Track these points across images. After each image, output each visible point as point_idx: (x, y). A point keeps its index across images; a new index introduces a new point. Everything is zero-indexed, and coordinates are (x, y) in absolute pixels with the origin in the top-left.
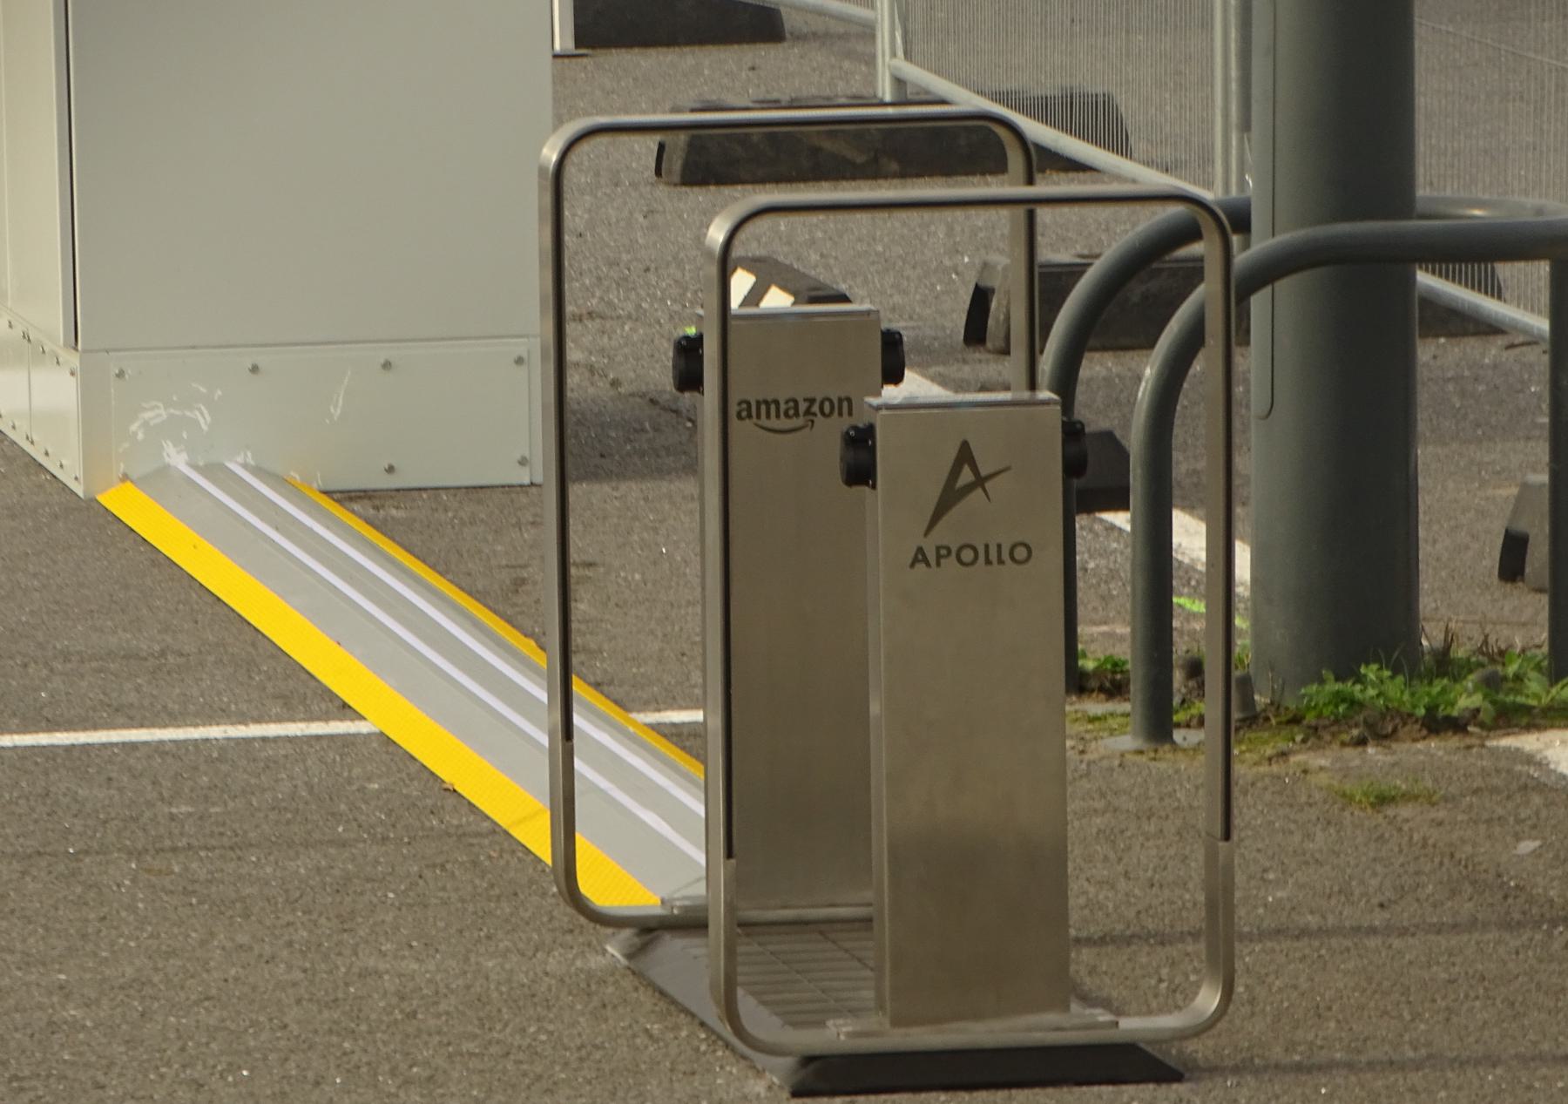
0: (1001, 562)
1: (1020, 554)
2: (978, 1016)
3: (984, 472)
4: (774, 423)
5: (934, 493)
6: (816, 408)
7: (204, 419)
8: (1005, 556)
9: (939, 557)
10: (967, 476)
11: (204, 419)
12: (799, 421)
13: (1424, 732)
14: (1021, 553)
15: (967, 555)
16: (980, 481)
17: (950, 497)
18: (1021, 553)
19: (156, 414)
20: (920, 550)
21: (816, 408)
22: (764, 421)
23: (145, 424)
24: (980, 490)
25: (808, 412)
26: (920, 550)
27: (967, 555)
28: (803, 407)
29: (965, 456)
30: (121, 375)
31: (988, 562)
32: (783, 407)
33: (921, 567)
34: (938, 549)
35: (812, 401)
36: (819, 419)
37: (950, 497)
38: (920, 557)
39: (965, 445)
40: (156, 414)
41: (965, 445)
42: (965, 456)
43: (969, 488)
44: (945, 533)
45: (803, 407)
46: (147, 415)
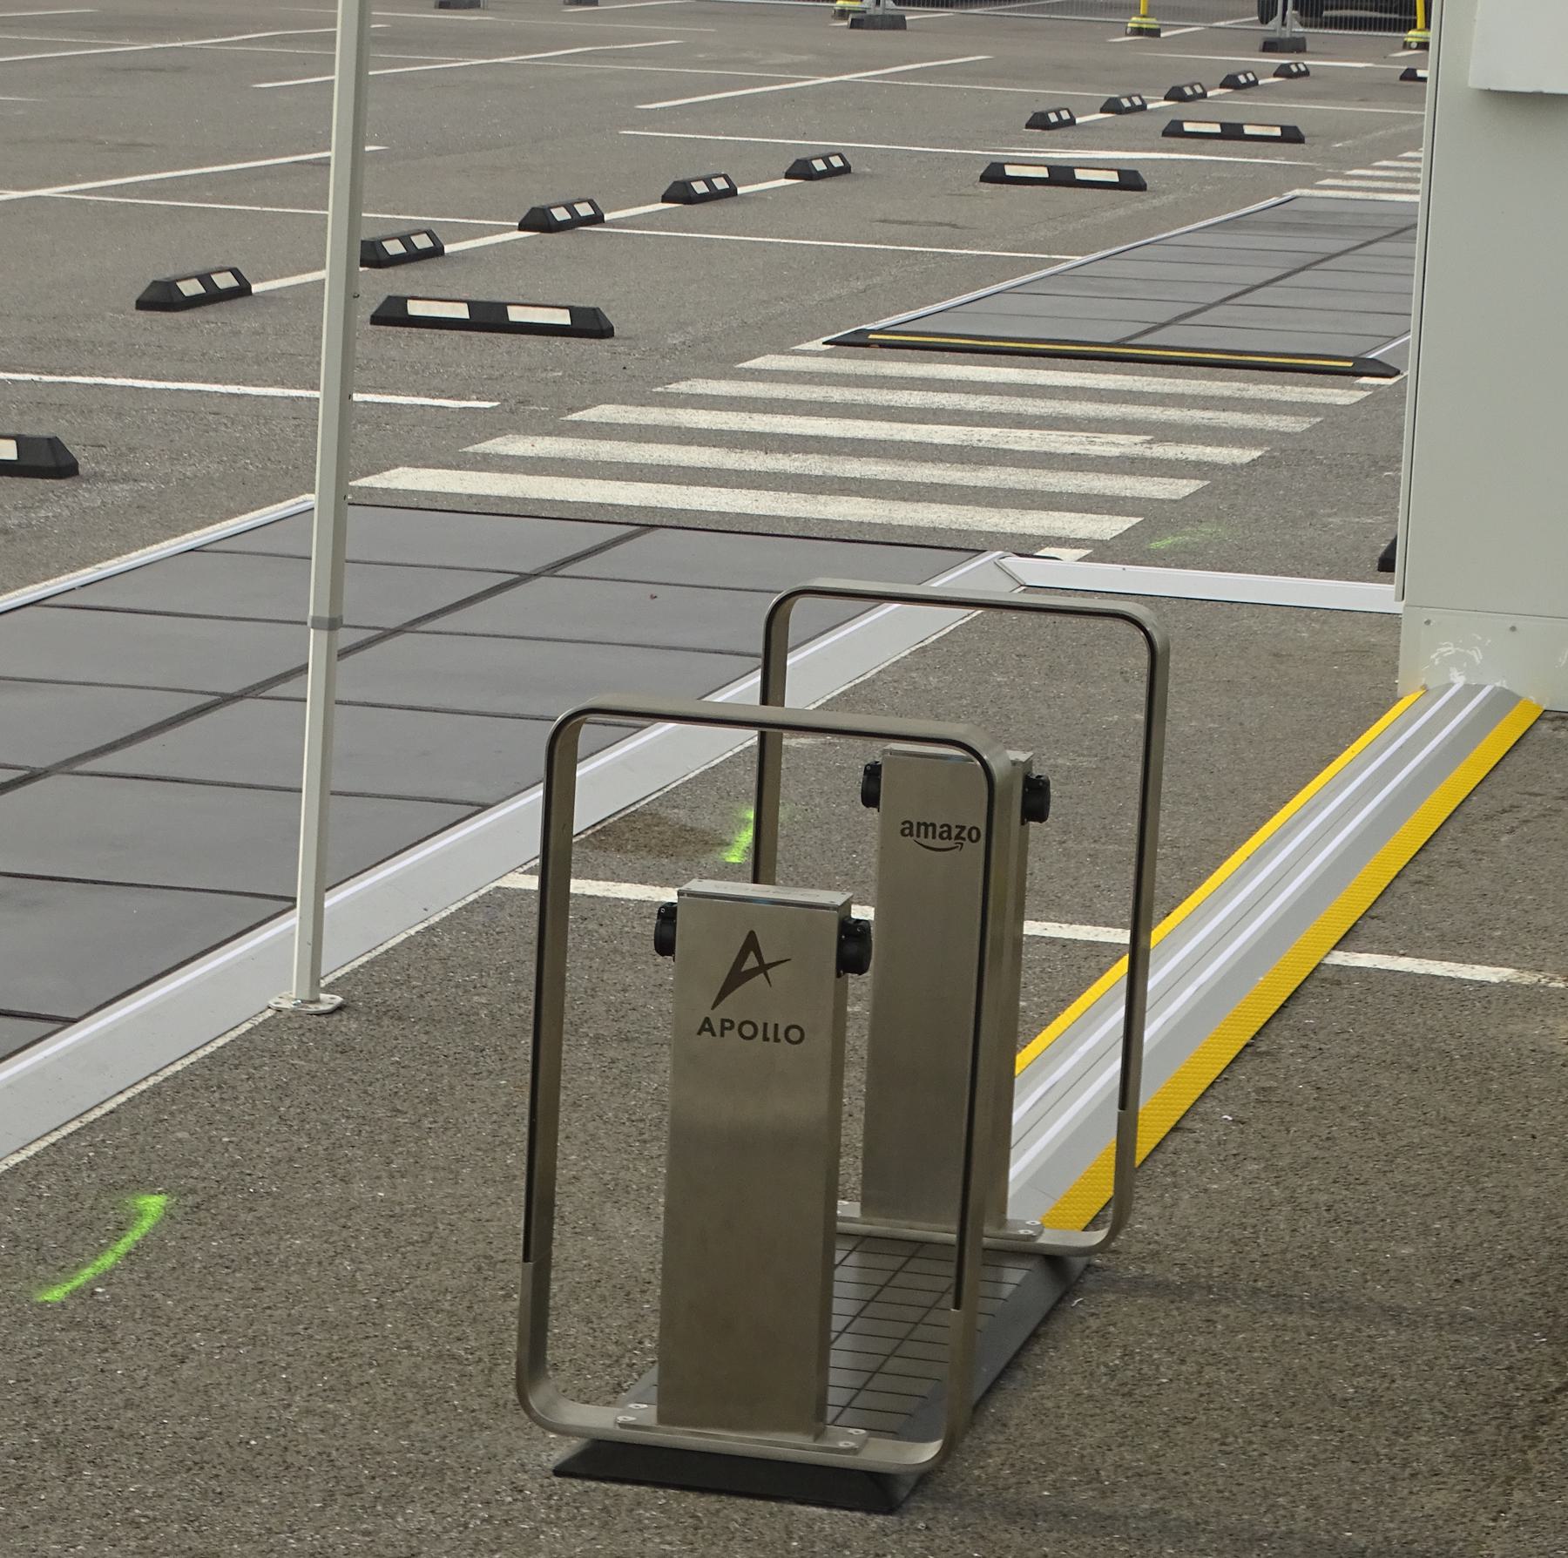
0: (777, 1040)
1: (795, 1034)
2: (731, 1426)
3: (766, 962)
4: (930, 842)
5: (722, 972)
6: (964, 834)
7: (1477, 656)
8: (781, 1035)
9: (723, 1028)
10: (751, 962)
11: (1477, 656)
12: (951, 843)
13: (1079, 1263)
14: (795, 1035)
15: (748, 1030)
16: (763, 968)
17: (736, 978)
18: (795, 1035)
19: (1448, 649)
20: (707, 1020)
21: (964, 834)
22: (922, 840)
23: (1440, 655)
24: (762, 975)
25: (958, 837)
26: (707, 1020)
27: (748, 1030)
28: (955, 832)
29: (751, 944)
30: (1428, 622)
31: (766, 1039)
32: (939, 830)
33: (706, 1034)
34: (723, 1021)
35: (963, 828)
36: (967, 843)
37: (736, 978)
38: (706, 1026)
39: (752, 935)
40: (1448, 649)
41: (752, 935)
42: (751, 944)
43: (753, 973)
44: (732, 1008)
45: (955, 832)
46: (1443, 650)
